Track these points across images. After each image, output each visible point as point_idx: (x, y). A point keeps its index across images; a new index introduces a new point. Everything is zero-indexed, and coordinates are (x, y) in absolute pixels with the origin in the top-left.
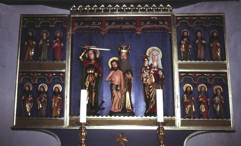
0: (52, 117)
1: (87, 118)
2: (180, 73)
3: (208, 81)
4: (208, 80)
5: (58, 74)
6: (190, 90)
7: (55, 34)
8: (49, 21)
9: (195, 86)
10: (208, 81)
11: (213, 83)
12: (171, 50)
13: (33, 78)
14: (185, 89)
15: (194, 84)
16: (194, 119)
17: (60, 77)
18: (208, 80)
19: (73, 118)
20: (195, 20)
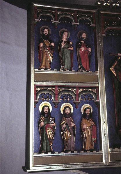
0: (114, 148)
1: (34, 156)
2: (36, 87)
3: (74, 98)
4: (73, 96)
5: (67, 89)
6: (69, 112)
7: (69, 33)
8: (52, 14)
9: (76, 106)
10: (74, 98)
11: (80, 101)
12: (95, 58)
13: (54, 95)
14: (63, 110)
15: (75, 103)
16: (59, 154)
17: (92, 94)
18: (73, 96)
19: (115, 151)
20: (40, 12)
